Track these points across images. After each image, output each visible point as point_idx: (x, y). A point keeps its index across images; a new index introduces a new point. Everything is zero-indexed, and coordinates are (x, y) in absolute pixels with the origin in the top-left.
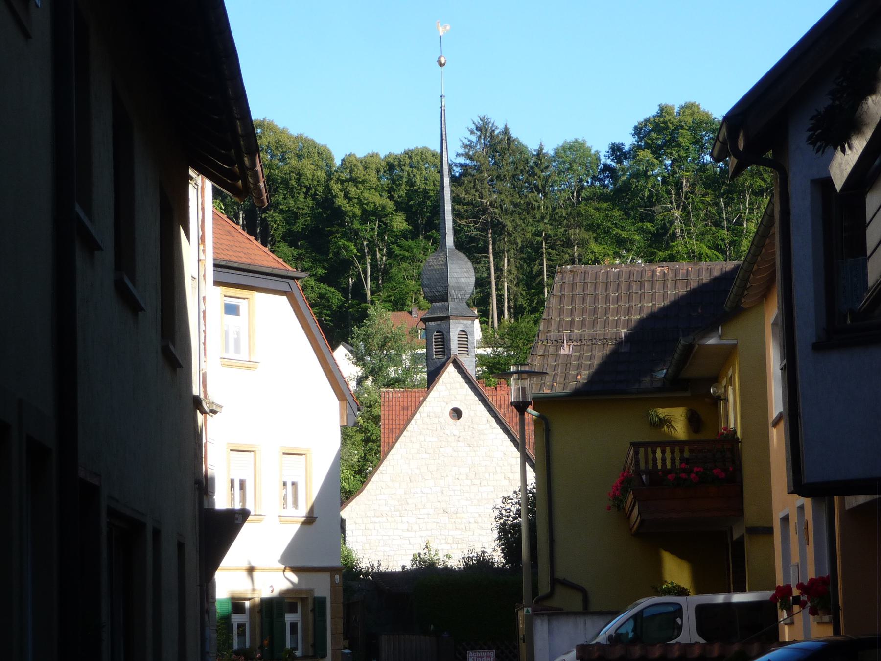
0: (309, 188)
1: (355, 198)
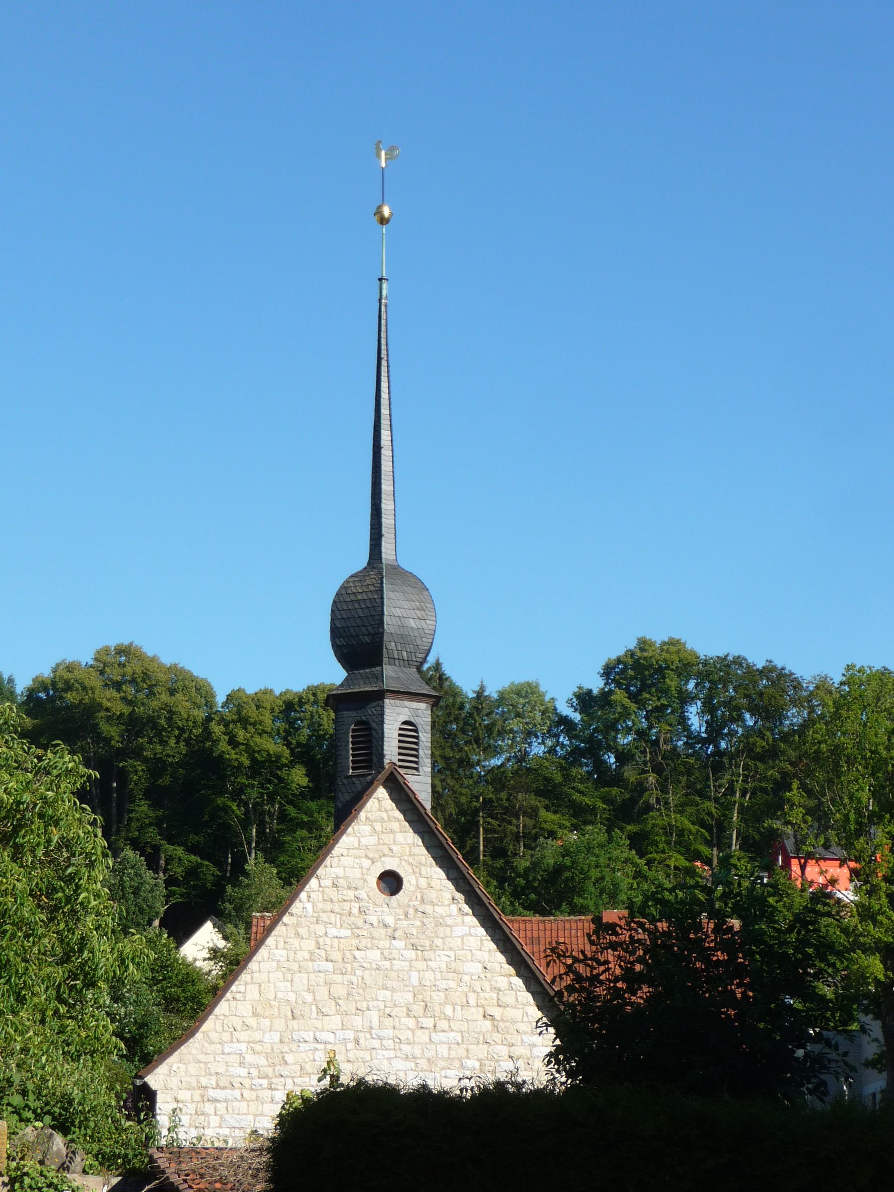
0: (182, 730)
1: (243, 744)
